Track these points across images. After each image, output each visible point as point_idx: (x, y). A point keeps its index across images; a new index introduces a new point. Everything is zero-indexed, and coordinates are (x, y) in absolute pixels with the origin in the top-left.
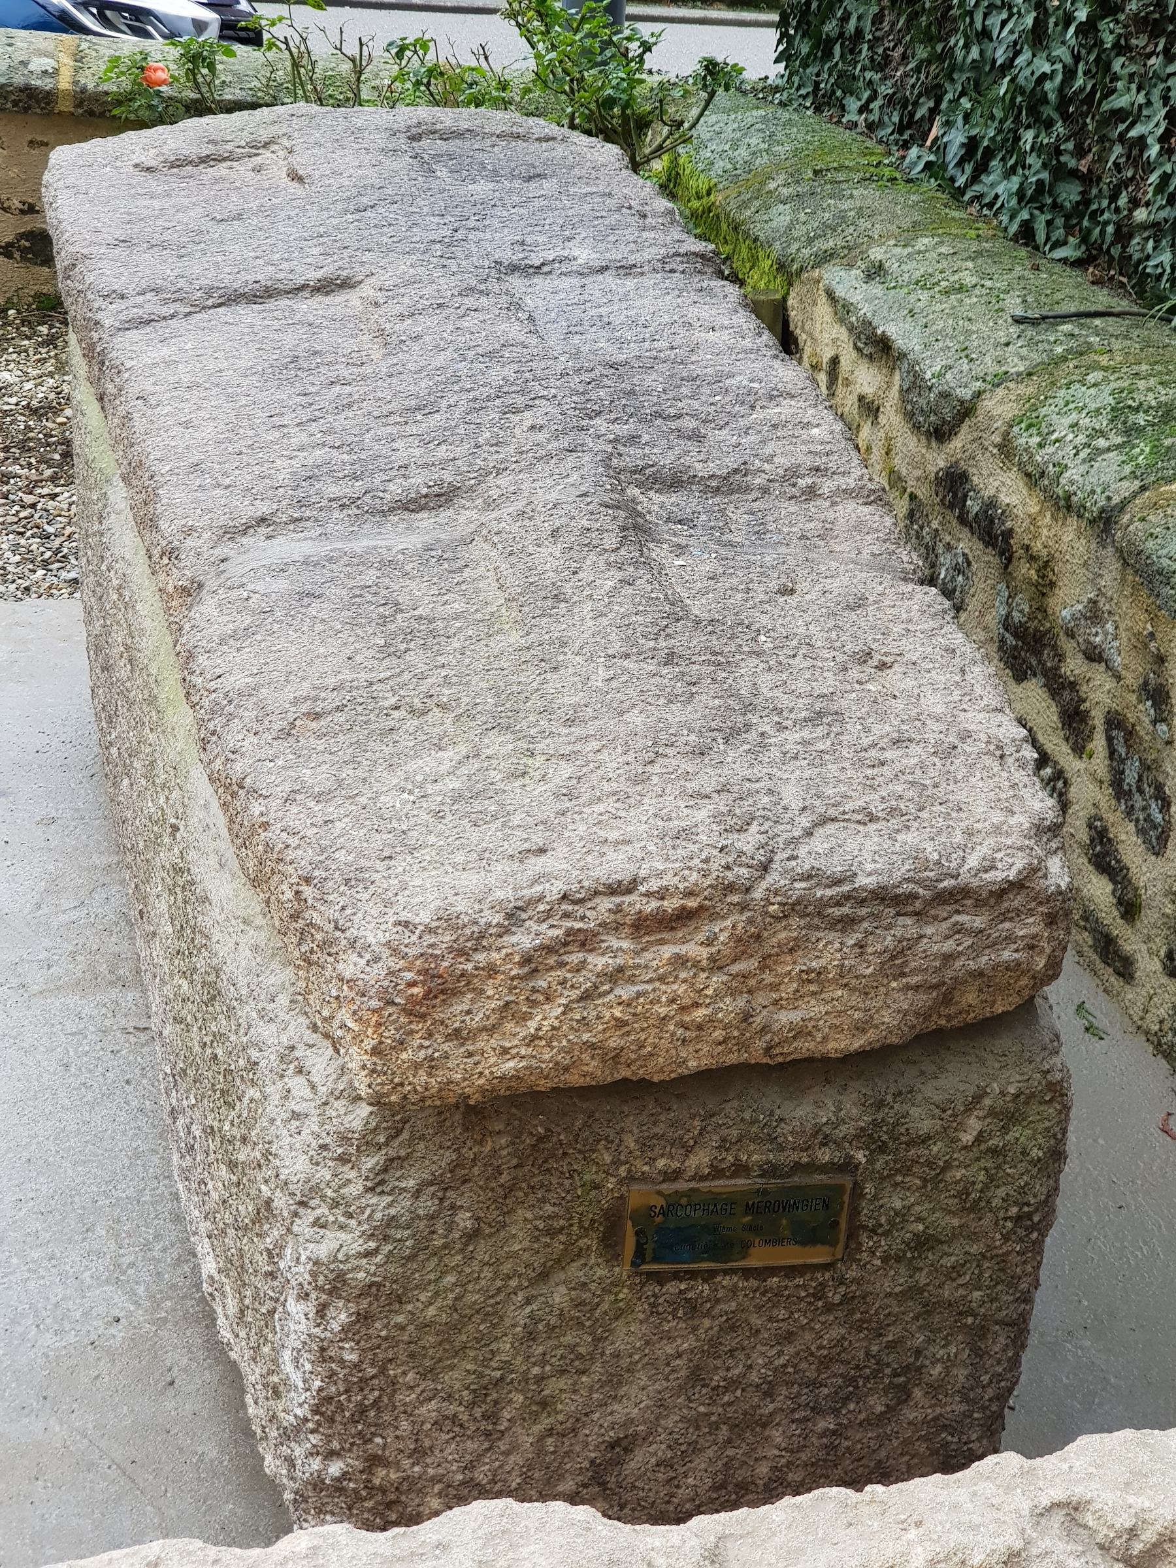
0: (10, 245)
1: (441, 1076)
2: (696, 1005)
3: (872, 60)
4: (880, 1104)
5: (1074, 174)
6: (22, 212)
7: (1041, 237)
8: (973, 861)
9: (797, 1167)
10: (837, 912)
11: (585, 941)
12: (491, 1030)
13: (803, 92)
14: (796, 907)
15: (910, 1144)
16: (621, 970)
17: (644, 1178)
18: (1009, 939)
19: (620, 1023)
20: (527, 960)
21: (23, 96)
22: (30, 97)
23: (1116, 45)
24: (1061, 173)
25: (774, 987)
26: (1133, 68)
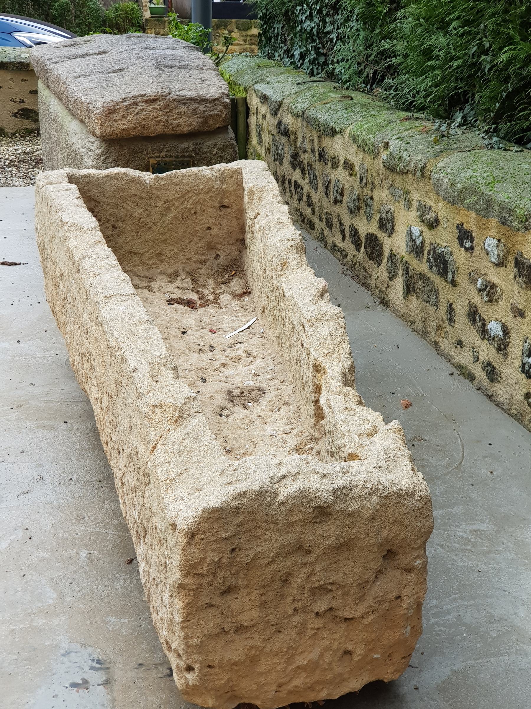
0: (16, 113)
1: (113, 129)
2: (158, 117)
3: (281, 41)
4: (197, 144)
5: (323, 54)
6: (20, 102)
7: (315, 73)
8: (209, 95)
9: (182, 156)
10: (183, 101)
11: (137, 104)
12: (121, 120)
13: (265, 55)
14: (175, 100)
15: (203, 153)
16: (143, 109)
17: (153, 157)
18: (216, 109)
19: (144, 119)
20: (126, 107)
21: (20, 65)
22: (21, 65)
23: (326, 14)
24: (319, 54)
25: (172, 116)
26: (330, 20)
